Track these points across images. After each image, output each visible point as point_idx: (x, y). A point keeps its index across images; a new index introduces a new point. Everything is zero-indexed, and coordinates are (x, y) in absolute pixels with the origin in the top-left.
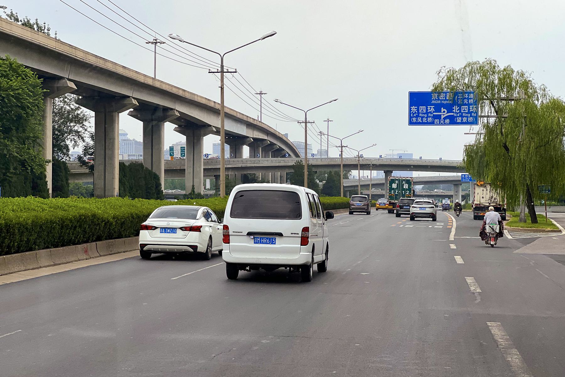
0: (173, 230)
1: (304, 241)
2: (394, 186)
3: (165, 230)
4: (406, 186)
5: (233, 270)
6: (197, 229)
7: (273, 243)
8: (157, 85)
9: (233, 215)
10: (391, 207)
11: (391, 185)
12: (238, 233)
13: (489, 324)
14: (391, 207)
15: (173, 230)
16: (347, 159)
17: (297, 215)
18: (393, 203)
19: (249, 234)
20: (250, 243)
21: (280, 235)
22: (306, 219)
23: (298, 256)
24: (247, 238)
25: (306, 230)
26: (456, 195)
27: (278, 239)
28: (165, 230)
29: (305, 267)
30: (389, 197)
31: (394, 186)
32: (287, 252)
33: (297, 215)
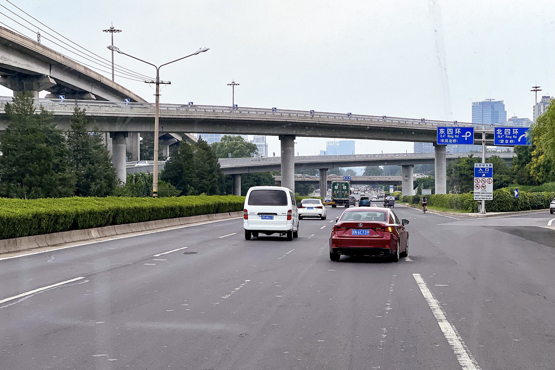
0: (312, 208)
1: (289, 218)
2: (336, 187)
3: (309, 208)
4: (345, 187)
5: (248, 234)
6: (321, 208)
7: (272, 218)
8: (115, 87)
9: (249, 204)
10: (334, 203)
11: (334, 187)
12: (253, 214)
13: (414, 275)
14: (334, 203)
15: (312, 208)
16: (299, 157)
17: (285, 203)
18: (336, 200)
19: (259, 214)
20: (259, 219)
21: (276, 214)
22: (290, 206)
23: (287, 226)
24: (258, 216)
25: (290, 211)
26: (406, 181)
27: (275, 216)
28: (309, 208)
29: (289, 232)
30: (333, 195)
31: (336, 187)
32: (280, 223)
33: (285, 203)
